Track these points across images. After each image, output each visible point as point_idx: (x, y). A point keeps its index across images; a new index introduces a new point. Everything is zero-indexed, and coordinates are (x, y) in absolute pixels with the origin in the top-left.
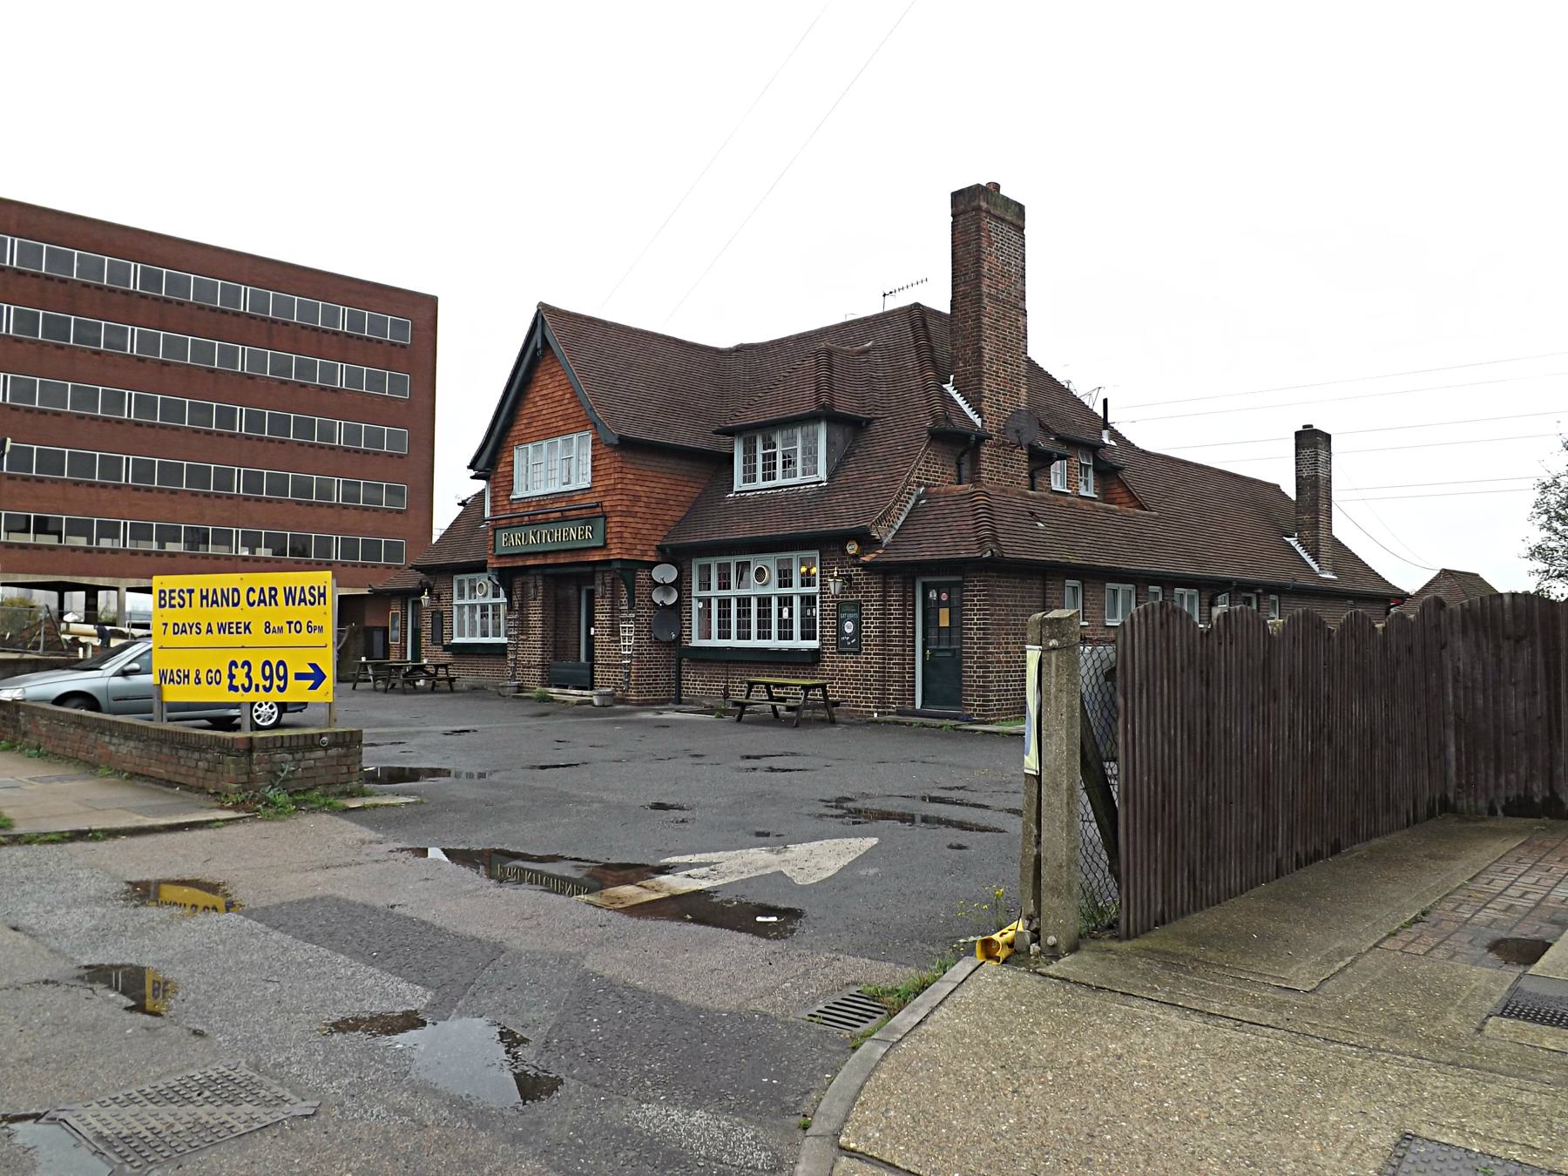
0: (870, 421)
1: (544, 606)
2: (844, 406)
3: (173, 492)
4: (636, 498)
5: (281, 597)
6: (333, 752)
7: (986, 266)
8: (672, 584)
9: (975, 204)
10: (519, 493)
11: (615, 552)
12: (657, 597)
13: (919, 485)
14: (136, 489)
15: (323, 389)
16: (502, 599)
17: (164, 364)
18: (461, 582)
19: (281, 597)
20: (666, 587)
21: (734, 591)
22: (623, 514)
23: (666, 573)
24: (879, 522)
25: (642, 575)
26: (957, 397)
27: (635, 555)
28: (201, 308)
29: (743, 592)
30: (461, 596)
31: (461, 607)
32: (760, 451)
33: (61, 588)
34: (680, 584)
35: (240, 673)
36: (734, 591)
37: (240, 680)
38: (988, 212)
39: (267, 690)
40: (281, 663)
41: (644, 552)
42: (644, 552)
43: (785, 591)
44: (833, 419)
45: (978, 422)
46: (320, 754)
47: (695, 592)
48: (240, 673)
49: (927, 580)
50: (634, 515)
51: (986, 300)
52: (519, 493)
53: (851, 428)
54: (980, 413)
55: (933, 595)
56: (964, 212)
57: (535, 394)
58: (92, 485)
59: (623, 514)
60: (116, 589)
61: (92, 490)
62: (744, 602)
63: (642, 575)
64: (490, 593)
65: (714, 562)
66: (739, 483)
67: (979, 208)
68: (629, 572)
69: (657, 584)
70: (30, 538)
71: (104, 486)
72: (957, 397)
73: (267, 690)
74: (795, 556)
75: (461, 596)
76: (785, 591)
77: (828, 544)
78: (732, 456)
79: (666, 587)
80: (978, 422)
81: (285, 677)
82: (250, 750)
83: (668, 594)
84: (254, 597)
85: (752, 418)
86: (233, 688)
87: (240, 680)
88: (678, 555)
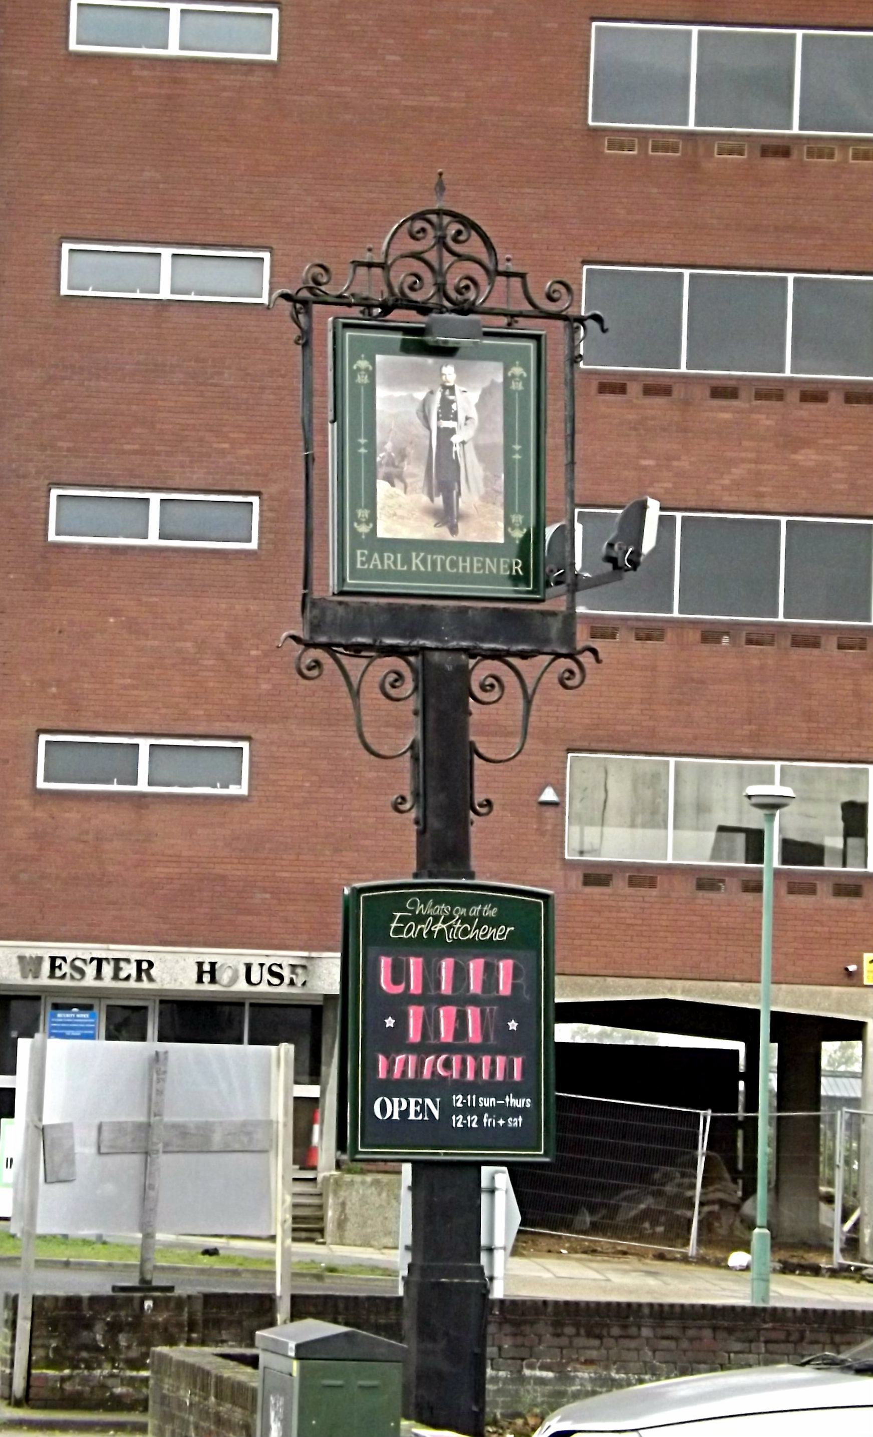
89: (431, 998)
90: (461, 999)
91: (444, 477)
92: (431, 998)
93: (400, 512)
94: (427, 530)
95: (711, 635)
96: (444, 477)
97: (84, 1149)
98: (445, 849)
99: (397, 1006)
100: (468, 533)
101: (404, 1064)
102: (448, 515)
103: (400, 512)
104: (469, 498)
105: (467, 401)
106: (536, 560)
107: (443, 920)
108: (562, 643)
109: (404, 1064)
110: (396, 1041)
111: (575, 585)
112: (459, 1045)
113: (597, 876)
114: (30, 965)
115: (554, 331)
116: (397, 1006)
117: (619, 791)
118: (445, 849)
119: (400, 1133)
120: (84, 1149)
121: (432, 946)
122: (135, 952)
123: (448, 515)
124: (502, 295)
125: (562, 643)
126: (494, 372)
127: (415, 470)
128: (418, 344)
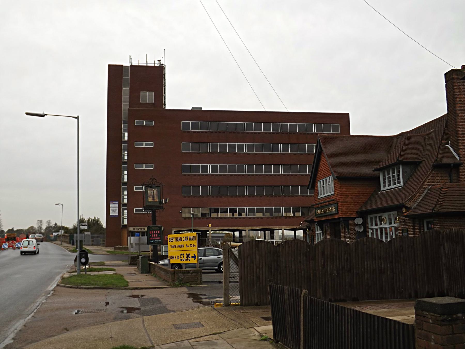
0: (420, 162)
1: (330, 233)
2: (409, 158)
3: (261, 196)
4: (347, 196)
5: (189, 239)
6: (193, 274)
7: (458, 99)
8: (361, 224)
9: (451, 77)
10: (320, 196)
11: (340, 215)
12: (357, 229)
13: (429, 185)
14: (249, 197)
15: (309, 154)
16: (321, 232)
17: (255, 154)
18: (371, 218)
19: (189, 239)
20: (360, 226)
21: (379, 226)
22: (342, 202)
23: (359, 221)
24: (409, 200)
25: (351, 222)
26: (451, 149)
27: (348, 215)
28: (266, 133)
29: (381, 226)
30: (372, 225)
31: (318, 234)
32: (387, 176)
33: (234, 231)
34: (365, 224)
35: (182, 256)
36: (393, 225)
37: (182, 258)
38: (458, 79)
39: (187, 260)
40: (189, 254)
41: (351, 214)
42: (351, 214)
43: (391, 226)
44: (405, 164)
45: (458, 158)
46: (190, 274)
47: (370, 227)
48: (182, 256)
49: (429, 220)
50: (346, 202)
51: (459, 112)
52: (320, 196)
53: (413, 165)
54: (459, 155)
55: (430, 226)
56: (449, 81)
57: (321, 163)
58: (236, 197)
59: (342, 202)
60: (245, 230)
61: (236, 198)
62: (381, 229)
63: (351, 222)
64: (388, 223)
65: (373, 216)
66: (382, 188)
67: (453, 79)
68: (347, 220)
69: (357, 225)
70: (220, 215)
71: (240, 197)
72: (451, 149)
73: (187, 260)
74: (391, 213)
75: (372, 225)
76: (391, 226)
77: (398, 208)
78: (380, 177)
79: (360, 226)
80: (458, 158)
81: (190, 257)
82: (174, 273)
83: (361, 228)
84: (184, 239)
85: (382, 165)
86: (181, 260)
87: (182, 258)
88: (363, 215)
89: (153, 234)
90: (156, 233)
91: (153, 197)
92: (153, 234)
93: (150, 200)
94: (152, 201)
95: (194, 197)
96: (153, 197)
97: (134, 245)
98: (154, 223)
99: (151, 234)
100: (155, 201)
101: (152, 238)
102: (154, 200)
103: (150, 200)
104: (155, 198)
105: (155, 191)
106: (161, 203)
107: (154, 228)
108: (162, 208)
109: (152, 238)
110: (151, 237)
111: (163, 204)
112: (156, 237)
113: (185, 219)
114: (134, 229)
115: (161, 186)
116: (151, 234)
117: (187, 211)
118: (154, 223)
119: (152, 243)
120: (134, 245)
121: (153, 230)
122: (143, 227)
123: (154, 200)
124: (157, 184)
125: (162, 208)
126: (157, 189)
127: (151, 197)
128: (151, 187)
